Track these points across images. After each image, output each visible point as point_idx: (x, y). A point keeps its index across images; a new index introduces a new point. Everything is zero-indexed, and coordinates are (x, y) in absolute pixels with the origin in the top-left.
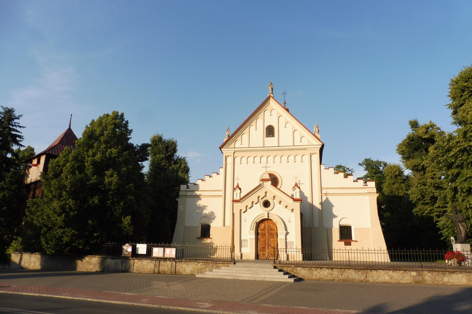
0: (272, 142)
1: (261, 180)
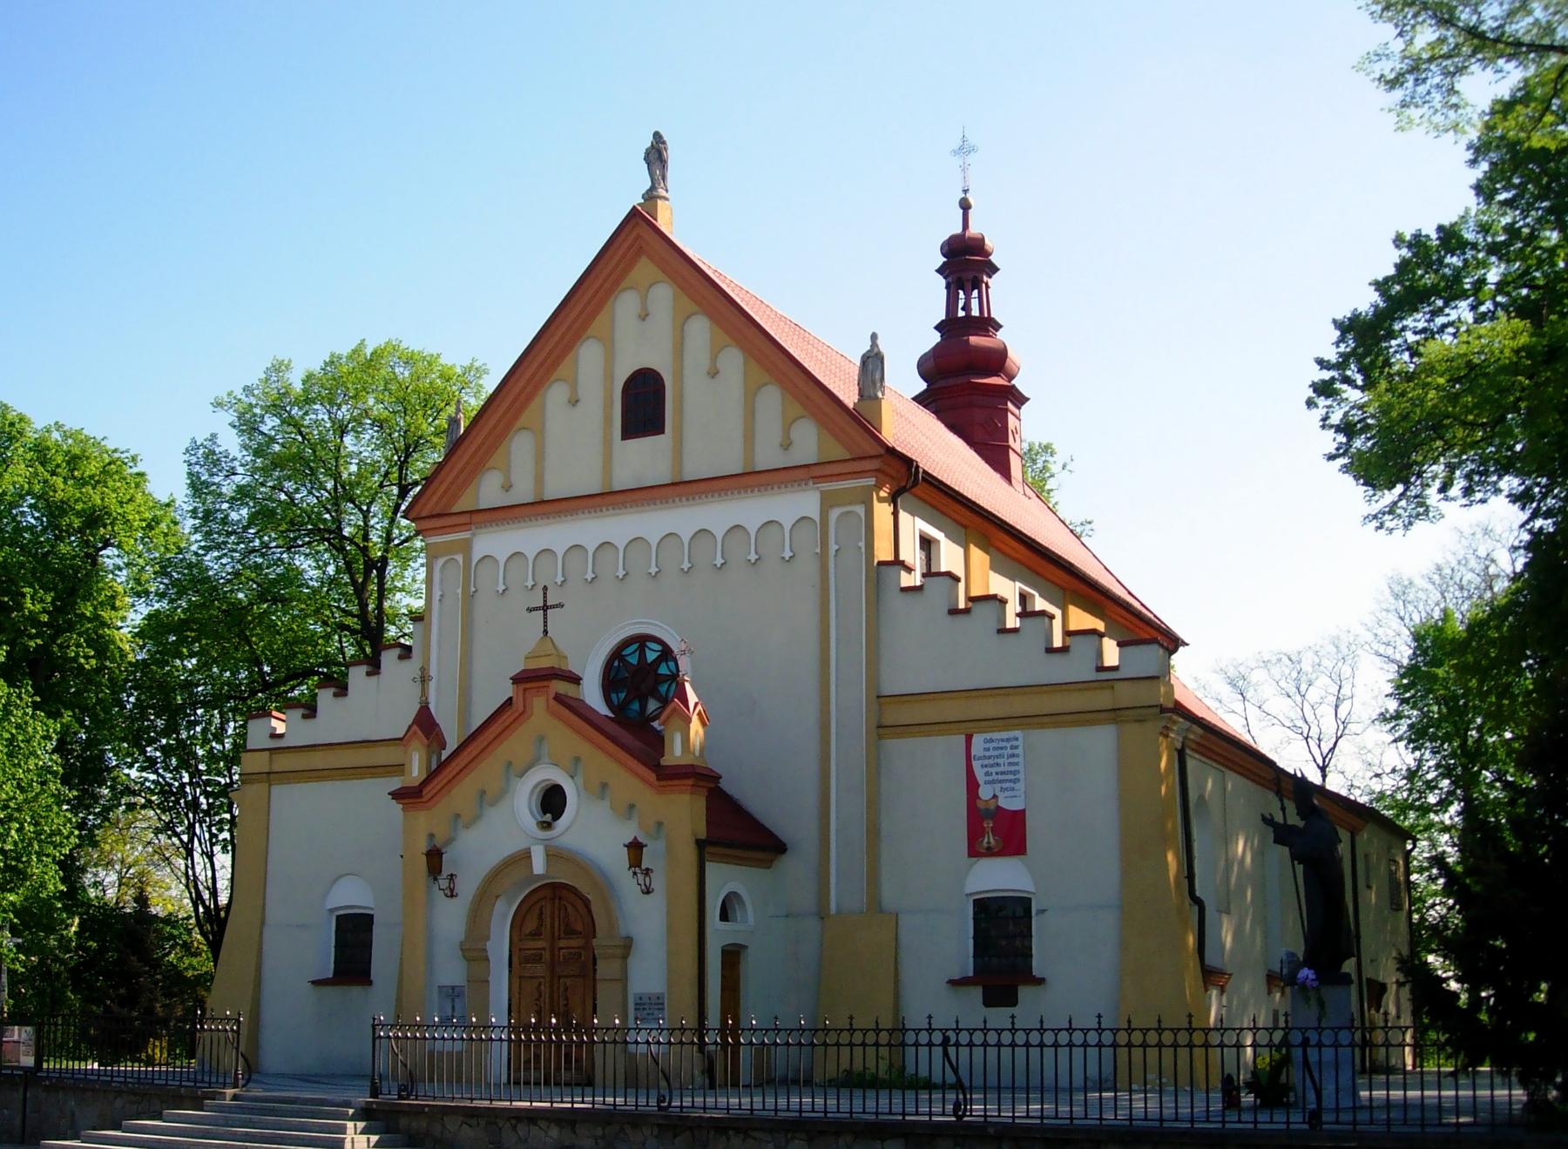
0: (644, 460)
1: (517, 680)
